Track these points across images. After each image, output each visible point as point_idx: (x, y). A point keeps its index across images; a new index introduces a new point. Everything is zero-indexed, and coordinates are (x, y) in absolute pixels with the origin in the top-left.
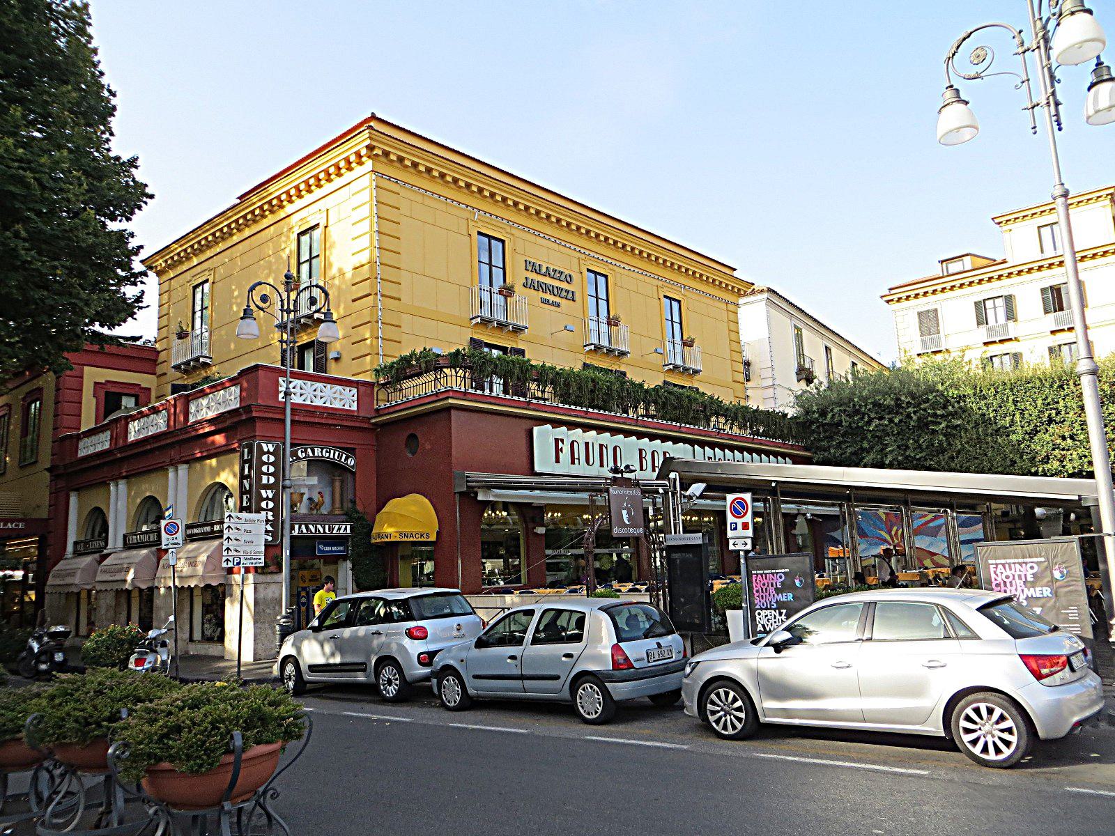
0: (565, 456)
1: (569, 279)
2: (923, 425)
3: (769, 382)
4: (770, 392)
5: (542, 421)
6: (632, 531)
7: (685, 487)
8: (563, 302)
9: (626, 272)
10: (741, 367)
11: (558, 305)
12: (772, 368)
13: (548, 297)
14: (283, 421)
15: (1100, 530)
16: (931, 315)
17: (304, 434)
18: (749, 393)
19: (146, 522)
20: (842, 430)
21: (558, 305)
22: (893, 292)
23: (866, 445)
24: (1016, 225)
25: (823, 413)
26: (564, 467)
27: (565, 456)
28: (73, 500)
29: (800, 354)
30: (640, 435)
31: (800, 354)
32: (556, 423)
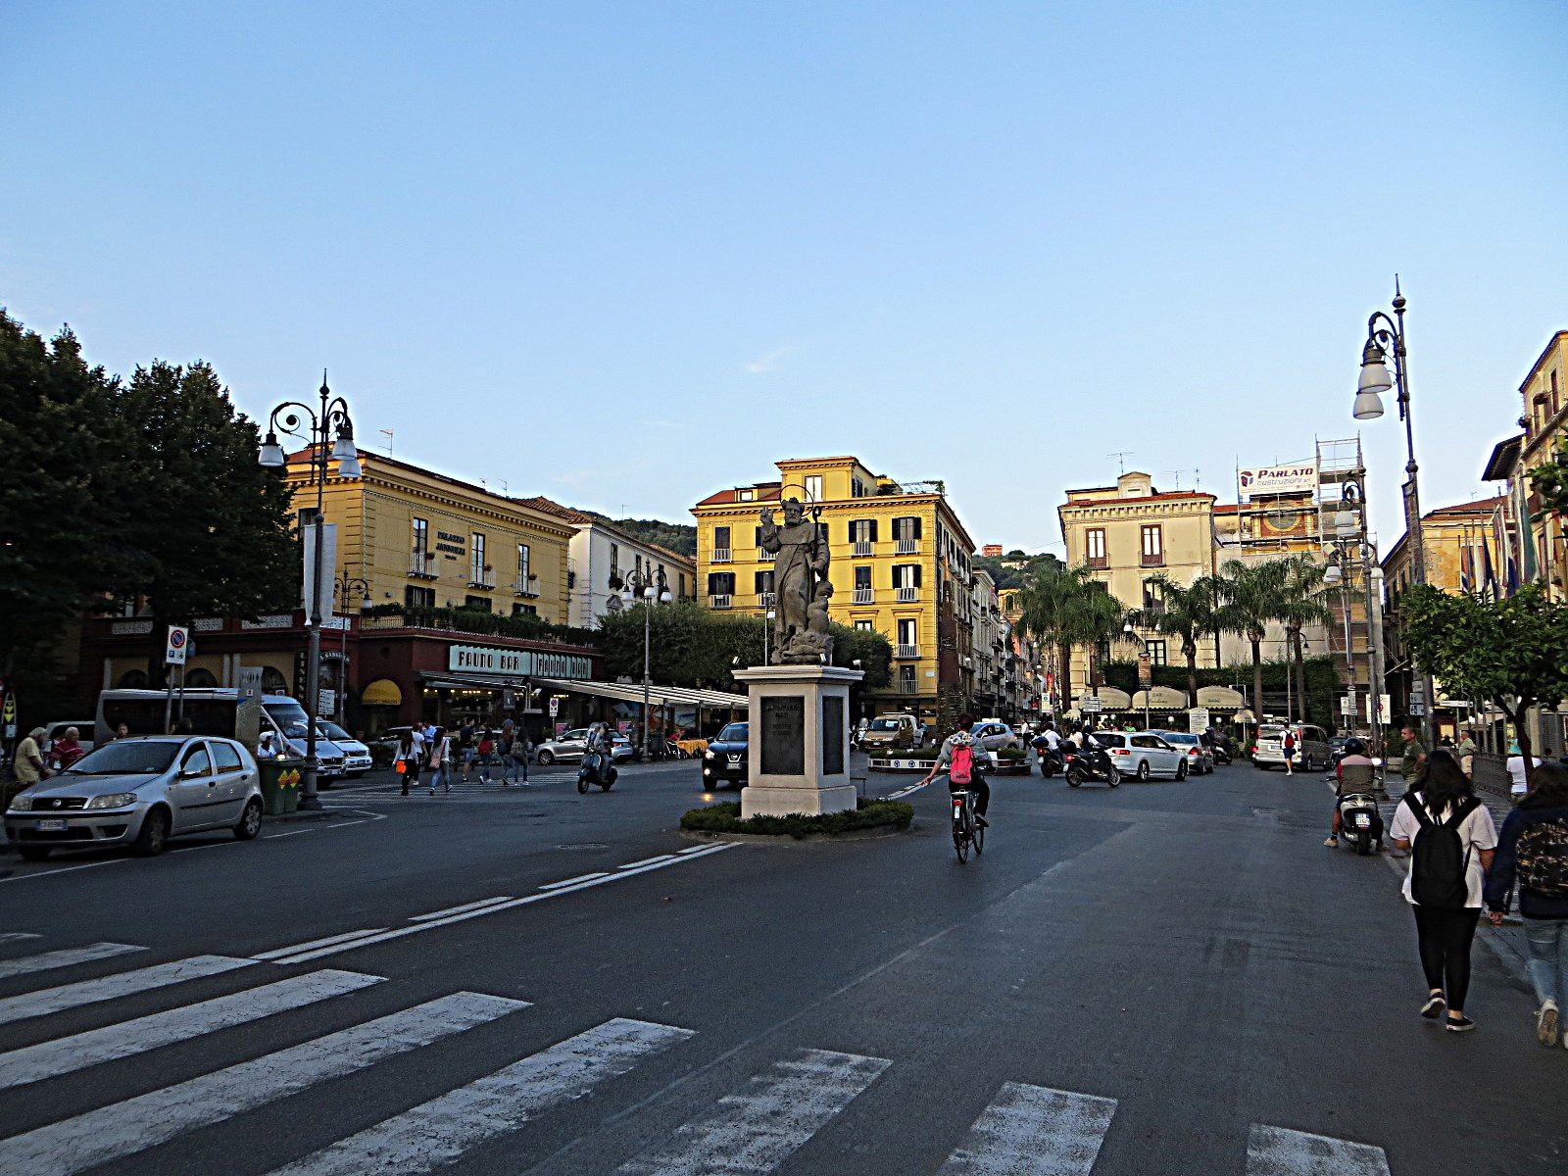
0: (464, 661)
1: (461, 540)
2: (669, 645)
3: (587, 591)
4: (586, 599)
5: (454, 643)
6: (511, 707)
7: (533, 690)
8: (458, 557)
9: (495, 531)
10: (566, 575)
11: (455, 558)
12: (590, 580)
13: (451, 554)
14: (341, 641)
15: (1145, 710)
16: (725, 532)
17: (327, 645)
18: (571, 597)
19: (999, 756)
20: (624, 643)
21: (455, 558)
22: (700, 507)
23: (636, 654)
24: (790, 472)
25: (614, 630)
26: (464, 667)
27: (464, 661)
28: (108, 663)
29: (614, 566)
30: (503, 649)
31: (614, 566)
32: (461, 644)
